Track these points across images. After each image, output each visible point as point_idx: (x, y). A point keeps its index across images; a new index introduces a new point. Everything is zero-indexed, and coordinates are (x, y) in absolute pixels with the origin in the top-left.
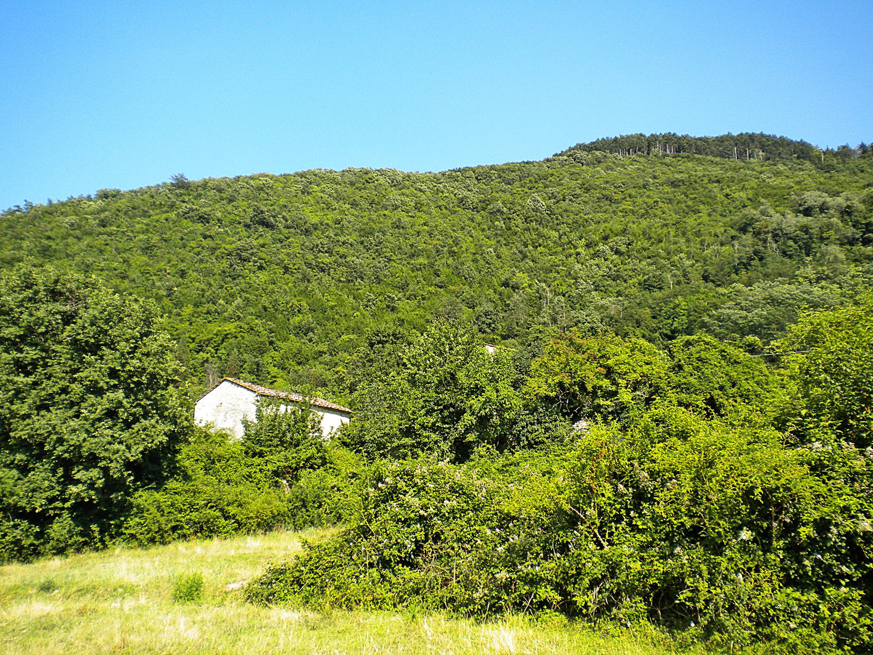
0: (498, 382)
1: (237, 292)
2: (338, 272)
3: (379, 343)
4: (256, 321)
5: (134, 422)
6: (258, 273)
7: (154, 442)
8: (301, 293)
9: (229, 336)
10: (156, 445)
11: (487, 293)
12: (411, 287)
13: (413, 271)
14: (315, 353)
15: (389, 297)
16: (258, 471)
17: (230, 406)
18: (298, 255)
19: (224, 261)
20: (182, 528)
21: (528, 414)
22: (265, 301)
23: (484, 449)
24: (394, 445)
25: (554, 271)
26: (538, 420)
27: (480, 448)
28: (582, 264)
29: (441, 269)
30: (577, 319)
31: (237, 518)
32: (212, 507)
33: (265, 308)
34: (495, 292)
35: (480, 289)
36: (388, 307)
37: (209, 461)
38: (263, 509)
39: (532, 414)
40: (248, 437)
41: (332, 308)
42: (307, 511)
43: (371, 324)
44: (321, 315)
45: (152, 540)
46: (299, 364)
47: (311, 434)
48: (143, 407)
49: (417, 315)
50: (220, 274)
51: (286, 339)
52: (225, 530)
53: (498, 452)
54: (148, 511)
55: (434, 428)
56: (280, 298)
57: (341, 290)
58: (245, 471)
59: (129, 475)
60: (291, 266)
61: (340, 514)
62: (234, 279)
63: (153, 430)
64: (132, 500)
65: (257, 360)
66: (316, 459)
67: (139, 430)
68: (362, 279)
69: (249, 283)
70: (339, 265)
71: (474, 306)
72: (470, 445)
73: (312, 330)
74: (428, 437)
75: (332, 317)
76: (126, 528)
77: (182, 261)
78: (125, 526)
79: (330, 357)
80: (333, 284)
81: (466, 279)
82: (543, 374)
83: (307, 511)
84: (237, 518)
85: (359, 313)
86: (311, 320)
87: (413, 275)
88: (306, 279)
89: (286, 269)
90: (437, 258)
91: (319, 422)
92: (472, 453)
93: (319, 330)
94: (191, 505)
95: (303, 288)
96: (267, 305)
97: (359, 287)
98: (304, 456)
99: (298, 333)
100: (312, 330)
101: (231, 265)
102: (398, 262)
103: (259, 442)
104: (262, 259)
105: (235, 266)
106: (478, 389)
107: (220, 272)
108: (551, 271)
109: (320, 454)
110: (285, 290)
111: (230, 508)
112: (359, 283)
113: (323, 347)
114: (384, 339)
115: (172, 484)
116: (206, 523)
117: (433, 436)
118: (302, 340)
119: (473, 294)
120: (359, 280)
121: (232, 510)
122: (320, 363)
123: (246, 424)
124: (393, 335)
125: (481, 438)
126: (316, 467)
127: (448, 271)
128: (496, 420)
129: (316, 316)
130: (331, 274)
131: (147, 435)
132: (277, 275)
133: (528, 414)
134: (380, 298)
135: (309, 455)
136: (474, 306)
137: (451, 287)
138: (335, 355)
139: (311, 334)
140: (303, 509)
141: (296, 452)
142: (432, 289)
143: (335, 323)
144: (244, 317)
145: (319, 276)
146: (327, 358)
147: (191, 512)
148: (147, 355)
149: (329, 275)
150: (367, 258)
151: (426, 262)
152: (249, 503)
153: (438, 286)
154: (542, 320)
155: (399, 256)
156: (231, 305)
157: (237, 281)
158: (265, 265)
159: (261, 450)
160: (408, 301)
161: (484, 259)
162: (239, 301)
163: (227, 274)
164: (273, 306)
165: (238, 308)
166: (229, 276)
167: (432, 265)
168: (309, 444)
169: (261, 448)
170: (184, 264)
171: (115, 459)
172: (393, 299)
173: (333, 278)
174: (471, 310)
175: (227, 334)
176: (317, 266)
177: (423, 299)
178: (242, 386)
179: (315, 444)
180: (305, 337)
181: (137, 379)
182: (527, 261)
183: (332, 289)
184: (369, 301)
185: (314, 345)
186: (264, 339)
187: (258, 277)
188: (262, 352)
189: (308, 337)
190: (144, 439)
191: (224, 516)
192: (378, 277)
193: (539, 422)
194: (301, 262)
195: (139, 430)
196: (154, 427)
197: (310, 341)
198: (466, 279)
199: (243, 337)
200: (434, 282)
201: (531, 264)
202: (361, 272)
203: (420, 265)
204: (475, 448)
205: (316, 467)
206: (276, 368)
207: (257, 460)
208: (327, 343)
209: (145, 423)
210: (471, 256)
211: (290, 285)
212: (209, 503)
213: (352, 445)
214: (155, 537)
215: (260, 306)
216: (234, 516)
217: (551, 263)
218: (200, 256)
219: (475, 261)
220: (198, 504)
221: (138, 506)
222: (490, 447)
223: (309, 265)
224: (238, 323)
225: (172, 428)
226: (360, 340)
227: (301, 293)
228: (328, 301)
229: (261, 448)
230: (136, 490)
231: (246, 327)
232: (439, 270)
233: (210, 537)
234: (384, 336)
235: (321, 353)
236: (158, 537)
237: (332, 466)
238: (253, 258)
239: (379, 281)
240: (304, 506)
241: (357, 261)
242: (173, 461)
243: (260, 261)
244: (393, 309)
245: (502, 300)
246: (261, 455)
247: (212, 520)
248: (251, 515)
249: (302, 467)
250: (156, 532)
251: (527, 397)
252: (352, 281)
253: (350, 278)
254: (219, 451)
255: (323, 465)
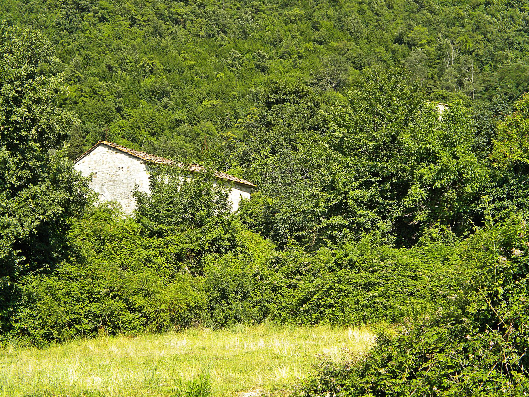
0: (455, 146)
1: (76, 48)
2: (196, 25)
3: (277, 102)
4: (101, 83)
5: (20, 188)
6: (100, 26)
7: (47, 214)
8: (152, 49)
9: (68, 102)
10: (49, 217)
11: (377, 50)
12: (284, 43)
13: (286, 24)
14: (171, 121)
15: (260, 55)
16: (157, 254)
17: (108, 176)
18: (147, 4)
19: (58, 10)
20: (80, 322)
21: (496, 187)
22: (110, 59)
23: (437, 230)
24: (323, 225)
25: (457, 24)
26: (508, 194)
27: (431, 229)
28: (493, 16)
29: (321, 22)
30: (489, 83)
31: (145, 310)
32: (114, 297)
33: (110, 68)
34: (387, 50)
35: (368, 46)
36: (258, 67)
37: (98, 241)
38: (178, 299)
39: (501, 187)
40: (142, 212)
41: (191, 68)
42: (228, 304)
43: (238, 88)
44: (178, 76)
45: (48, 337)
46: (153, 134)
47: (216, 210)
48: (32, 170)
49: (293, 76)
50: (53, 27)
51: (135, 106)
52: (132, 325)
53: (454, 234)
54: (41, 300)
55: (371, 205)
56: (128, 56)
57: (201, 46)
58: (144, 254)
59: (19, 254)
60: (139, 17)
61: (267, 309)
62: (72, 32)
63: (45, 198)
64: (20, 287)
65: (103, 129)
66: (223, 241)
67: (28, 198)
68: (225, 32)
69: (89, 38)
70: (197, 16)
71: (361, 66)
72: (419, 227)
73: (168, 94)
74: (365, 216)
75: (190, 79)
76: (16, 321)
77: (7, 11)
78: (13, 318)
79: (190, 127)
80: (190, 39)
81: (351, 33)
82: (515, 136)
83: (228, 304)
84: (145, 310)
85: (222, 74)
86: (166, 82)
87: (286, 28)
88: (157, 32)
89: (133, 22)
90: (316, 7)
91: (227, 195)
92: (421, 235)
93: (175, 95)
94: (90, 295)
95: (154, 44)
96: (112, 63)
97: (222, 43)
98: (209, 237)
99: (150, 98)
100: (168, 94)
101: (67, 16)
102: (268, 12)
103: (157, 219)
104: (103, 9)
105: (71, 17)
106: (430, 154)
107: (54, 24)
108: (454, 24)
109: (228, 235)
110: (133, 46)
111: (135, 298)
112: (222, 37)
113: (181, 115)
114: (284, 97)
115: (64, 267)
116: (109, 316)
117: (370, 213)
118: (156, 107)
119: (360, 51)
120: (222, 34)
121: (139, 301)
122: (179, 134)
123: (139, 198)
124: (295, 93)
125: (433, 216)
126: (224, 250)
127: (328, 23)
128: (451, 194)
129: (171, 77)
130: (188, 27)
131: (37, 204)
132: (122, 29)
133: (496, 187)
134: (247, 56)
135: (215, 236)
136: (361, 66)
137: (334, 44)
138: (196, 124)
139: (166, 99)
140: (224, 302)
141: (201, 233)
142: (310, 45)
143: (194, 87)
144: (85, 78)
145: (173, 29)
146: (186, 127)
147: (90, 302)
148: (38, 102)
149: (185, 28)
150: (231, 8)
151: (302, 13)
152: (159, 292)
153: (317, 41)
154: (445, 84)
155: (270, 6)
156: (69, 64)
157: (75, 35)
158: (107, 16)
159: (160, 229)
160: (282, 60)
161: (372, 9)
162: (77, 59)
163: (63, 27)
164: (120, 66)
165: (77, 67)
166: (65, 29)
167: (309, 17)
168: (214, 222)
169: (159, 226)
170: (10, 14)
171: (6, 235)
172: (264, 57)
173: (190, 32)
174: (358, 71)
175: (66, 99)
176: (170, 17)
177: (300, 57)
178: (122, 152)
179: (223, 222)
180: (159, 103)
181: (25, 133)
182: (425, 12)
183: (190, 45)
184: (234, 60)
185: (171, 112)
186: (110, 104)
187: (100, 30)
188: (109, 121)
189: (163, 103)
190: (33, 210)
191: (129, 308)
192: (244, 31)
193: (510, 197)
194: (151, 12)
195: (28, 198)
196: (45, 194)
197: (166, 107)
198: (351, 33)
199: (84, 102)
200: (313, 37)
201: (429, 15)
202: (224, 25)
203: (295, 16)
204: (426, 230)
205: (224, 250)
206: (125, 140)
207: (155, 241)
208: (186, 110)
209: (33, 188)
210: (356, 6)
211: (139, 40)
212: (111, 291)
213: (255, 226)
214: (51, 334)
215: (104, 66)
216: (141, 309)
217: (454, 15)
218: (29, 5)
219: (361, 12)
220: (99, 293)
221: (29, 295)
222: (445, 227)
223: (161, 16)
224: (78, 85)
225: (66, 196)
226: (224, 107)
227: (152, 49)
228: (185, 59)
229: (159, 226)
230: (22, 274)
231: (88, 90)
232: (318, 23)
233: (114, 334)
234: (284, 94)
235: (179, 122)
236: (55, 334)
237: (243, 249)
238: (94, 7)
239: (246, 36)
240: (224, 296)
241: (219, 11)
242: (62, 240)
243: (101, 11)
244: (264, 70)
245: (395, 60)
246: (160, 234)
247: (116, 313)
248: (163, 307)
249: (207, 251)
250: (53, 327)
251: (495, 165)
252: (213, 36)
253: (210, 32)
254: (109, 228)
255: (232, 248)
